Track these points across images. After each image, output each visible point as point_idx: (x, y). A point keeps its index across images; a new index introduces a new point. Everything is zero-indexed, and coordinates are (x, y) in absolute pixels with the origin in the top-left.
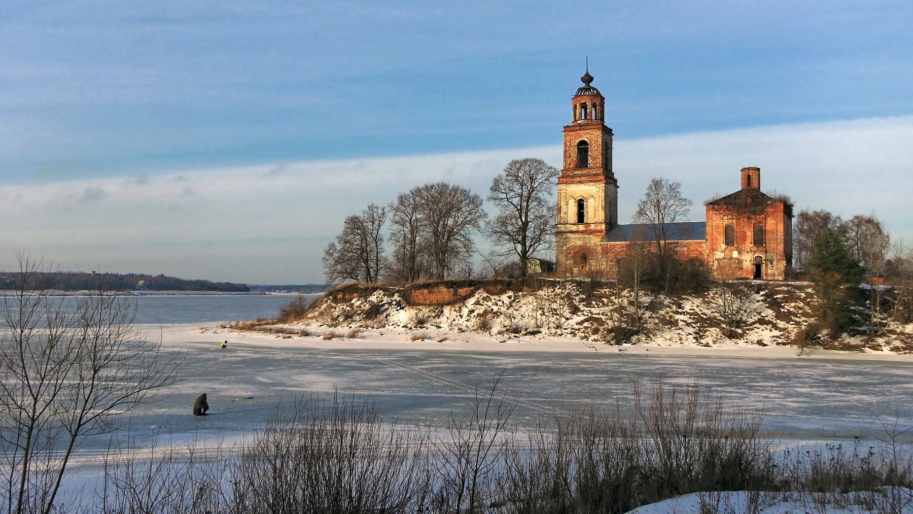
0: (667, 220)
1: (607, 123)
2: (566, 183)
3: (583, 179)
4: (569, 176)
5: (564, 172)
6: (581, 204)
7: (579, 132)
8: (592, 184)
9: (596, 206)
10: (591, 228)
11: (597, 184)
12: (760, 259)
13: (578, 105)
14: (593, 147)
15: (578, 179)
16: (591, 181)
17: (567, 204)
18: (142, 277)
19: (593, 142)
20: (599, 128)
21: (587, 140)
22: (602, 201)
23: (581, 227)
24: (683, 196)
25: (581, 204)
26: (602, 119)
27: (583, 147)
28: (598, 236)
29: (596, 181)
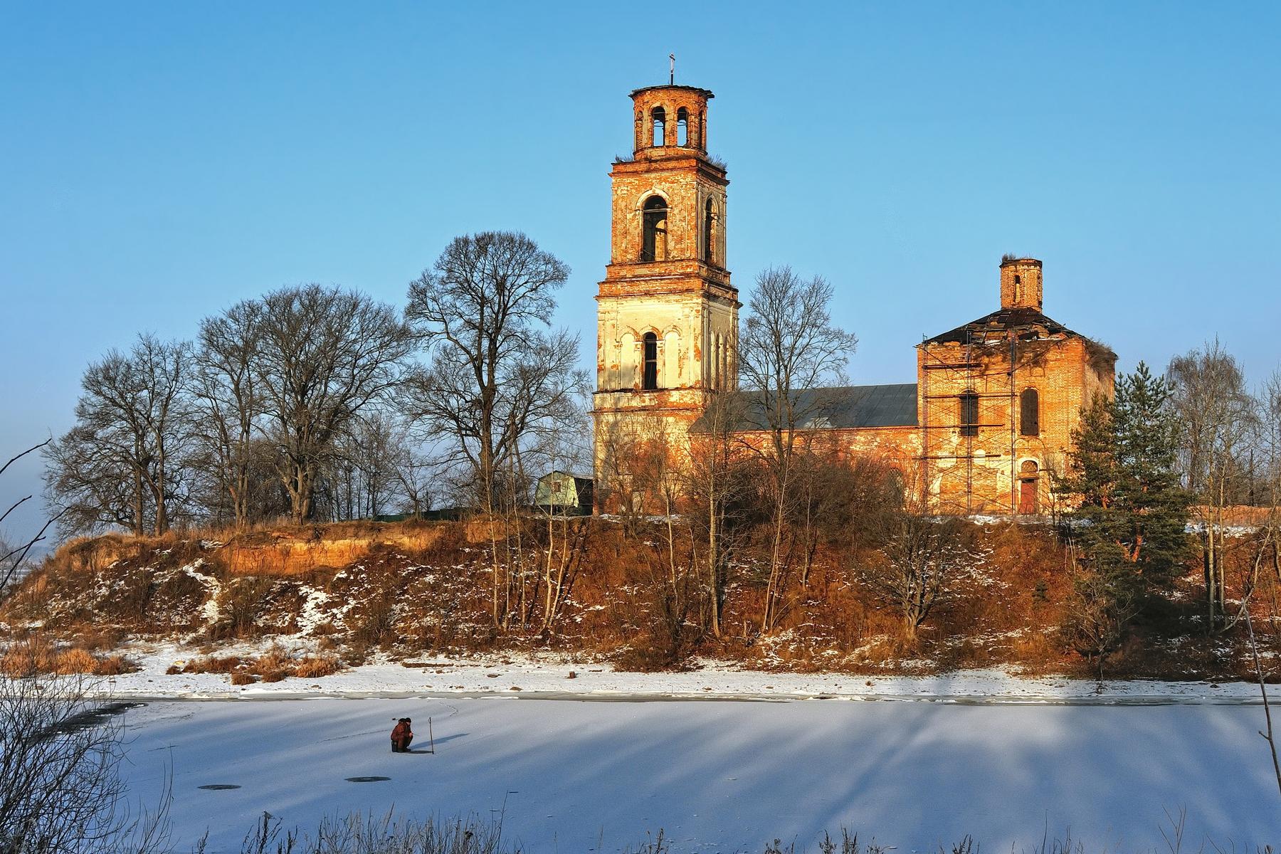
0: (796, 385)
1: (715, 153)
2: (616, 296)
3: (656, 285)
4: (622, 279)
5: (612, 269)
6: (650, 343)
7: (646, 175)
8: (677, 297)
9: (683, 350)
10: (672, 399)
11: (686, 296)
12: (1032, 467)
13: (646, 114)
14: (676, 211)
15: (643, 287)
16: (672, 292)
17: (619, 345)
18: (1051, 321)
19: (677, 199)
20: (690, 169)
21: (664, 195)
22: (696, 338)
23: (648, 399)
24: (833, 325)
25: (650, 343)
26: (700, 146)
27: (655, 209)
28: (682, 418)
29: (682, 292)
